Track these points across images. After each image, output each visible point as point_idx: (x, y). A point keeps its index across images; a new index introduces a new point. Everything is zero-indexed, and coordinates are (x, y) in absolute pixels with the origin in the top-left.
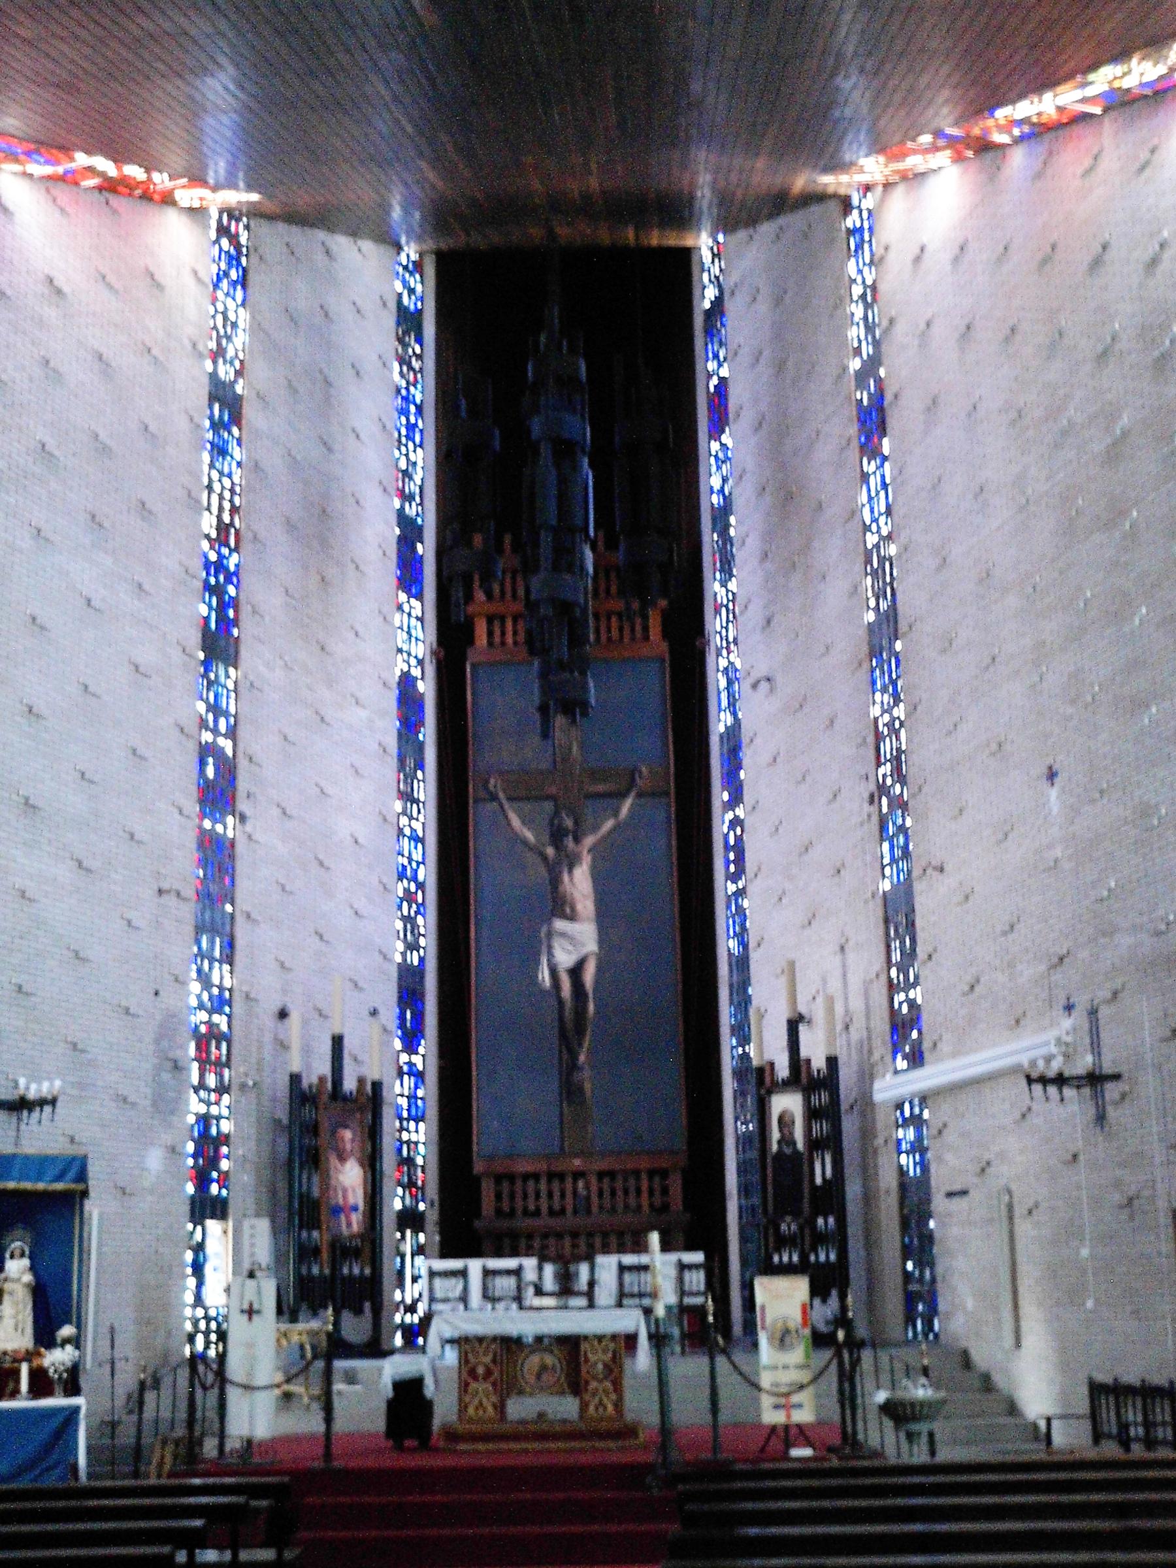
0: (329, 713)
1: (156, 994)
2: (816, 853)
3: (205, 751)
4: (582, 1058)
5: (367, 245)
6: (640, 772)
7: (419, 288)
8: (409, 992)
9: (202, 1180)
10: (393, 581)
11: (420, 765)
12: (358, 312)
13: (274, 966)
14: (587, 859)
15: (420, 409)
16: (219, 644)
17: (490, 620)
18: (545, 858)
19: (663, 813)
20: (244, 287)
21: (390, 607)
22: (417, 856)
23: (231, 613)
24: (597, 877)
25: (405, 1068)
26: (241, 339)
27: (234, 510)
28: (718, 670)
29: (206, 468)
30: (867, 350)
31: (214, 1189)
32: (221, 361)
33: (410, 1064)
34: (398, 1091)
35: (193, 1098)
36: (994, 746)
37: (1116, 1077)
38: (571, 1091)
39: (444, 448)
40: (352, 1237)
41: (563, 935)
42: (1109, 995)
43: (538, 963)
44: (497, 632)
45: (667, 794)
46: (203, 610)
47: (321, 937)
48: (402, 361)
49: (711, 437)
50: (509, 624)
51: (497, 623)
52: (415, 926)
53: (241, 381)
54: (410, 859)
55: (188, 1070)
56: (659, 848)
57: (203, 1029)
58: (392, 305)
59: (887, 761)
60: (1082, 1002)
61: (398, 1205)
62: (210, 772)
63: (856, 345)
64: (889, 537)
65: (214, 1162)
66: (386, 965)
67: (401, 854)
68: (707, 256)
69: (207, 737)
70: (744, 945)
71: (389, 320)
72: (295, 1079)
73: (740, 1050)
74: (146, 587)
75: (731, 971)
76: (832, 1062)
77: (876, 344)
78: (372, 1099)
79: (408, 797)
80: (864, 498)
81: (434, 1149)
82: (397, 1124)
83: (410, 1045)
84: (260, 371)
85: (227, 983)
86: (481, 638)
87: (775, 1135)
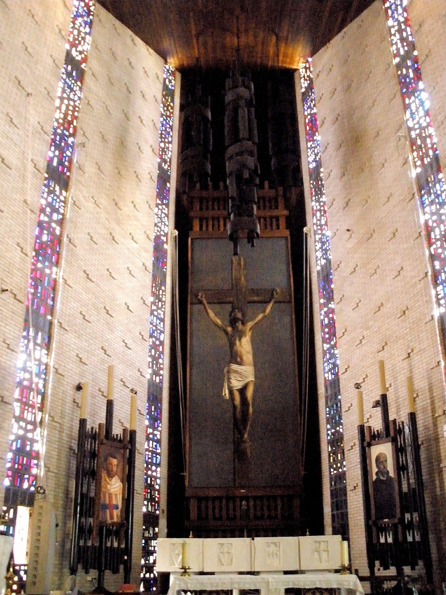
4: (246, 436)
5: (151, 51)
6: (276, 290)
7: (173, 81)
8: (154, 398)
10: (155, 194)
14: (249, 334)
17: (201, 220)
20: (90, 27)
21: (153, 205)
29: (60, 90)
35: (16, 426)
38: (239, 454)
39: (180, 161)
40: (113, 524)
41: (236, 372)
43: (222, 386)
45: (290, 302)
46: (51, 154)
49: (307, 141)
50: (211, 223)
51: (204, 221)
61: (144, 509)
65: (27, 468)
68: (302, 71)
69: (43, 218)
70: (336, 375)
72: (83, 422)
74: (14, 121)
76: (413, 416)
78: (128, 442)
87: (375, 469)
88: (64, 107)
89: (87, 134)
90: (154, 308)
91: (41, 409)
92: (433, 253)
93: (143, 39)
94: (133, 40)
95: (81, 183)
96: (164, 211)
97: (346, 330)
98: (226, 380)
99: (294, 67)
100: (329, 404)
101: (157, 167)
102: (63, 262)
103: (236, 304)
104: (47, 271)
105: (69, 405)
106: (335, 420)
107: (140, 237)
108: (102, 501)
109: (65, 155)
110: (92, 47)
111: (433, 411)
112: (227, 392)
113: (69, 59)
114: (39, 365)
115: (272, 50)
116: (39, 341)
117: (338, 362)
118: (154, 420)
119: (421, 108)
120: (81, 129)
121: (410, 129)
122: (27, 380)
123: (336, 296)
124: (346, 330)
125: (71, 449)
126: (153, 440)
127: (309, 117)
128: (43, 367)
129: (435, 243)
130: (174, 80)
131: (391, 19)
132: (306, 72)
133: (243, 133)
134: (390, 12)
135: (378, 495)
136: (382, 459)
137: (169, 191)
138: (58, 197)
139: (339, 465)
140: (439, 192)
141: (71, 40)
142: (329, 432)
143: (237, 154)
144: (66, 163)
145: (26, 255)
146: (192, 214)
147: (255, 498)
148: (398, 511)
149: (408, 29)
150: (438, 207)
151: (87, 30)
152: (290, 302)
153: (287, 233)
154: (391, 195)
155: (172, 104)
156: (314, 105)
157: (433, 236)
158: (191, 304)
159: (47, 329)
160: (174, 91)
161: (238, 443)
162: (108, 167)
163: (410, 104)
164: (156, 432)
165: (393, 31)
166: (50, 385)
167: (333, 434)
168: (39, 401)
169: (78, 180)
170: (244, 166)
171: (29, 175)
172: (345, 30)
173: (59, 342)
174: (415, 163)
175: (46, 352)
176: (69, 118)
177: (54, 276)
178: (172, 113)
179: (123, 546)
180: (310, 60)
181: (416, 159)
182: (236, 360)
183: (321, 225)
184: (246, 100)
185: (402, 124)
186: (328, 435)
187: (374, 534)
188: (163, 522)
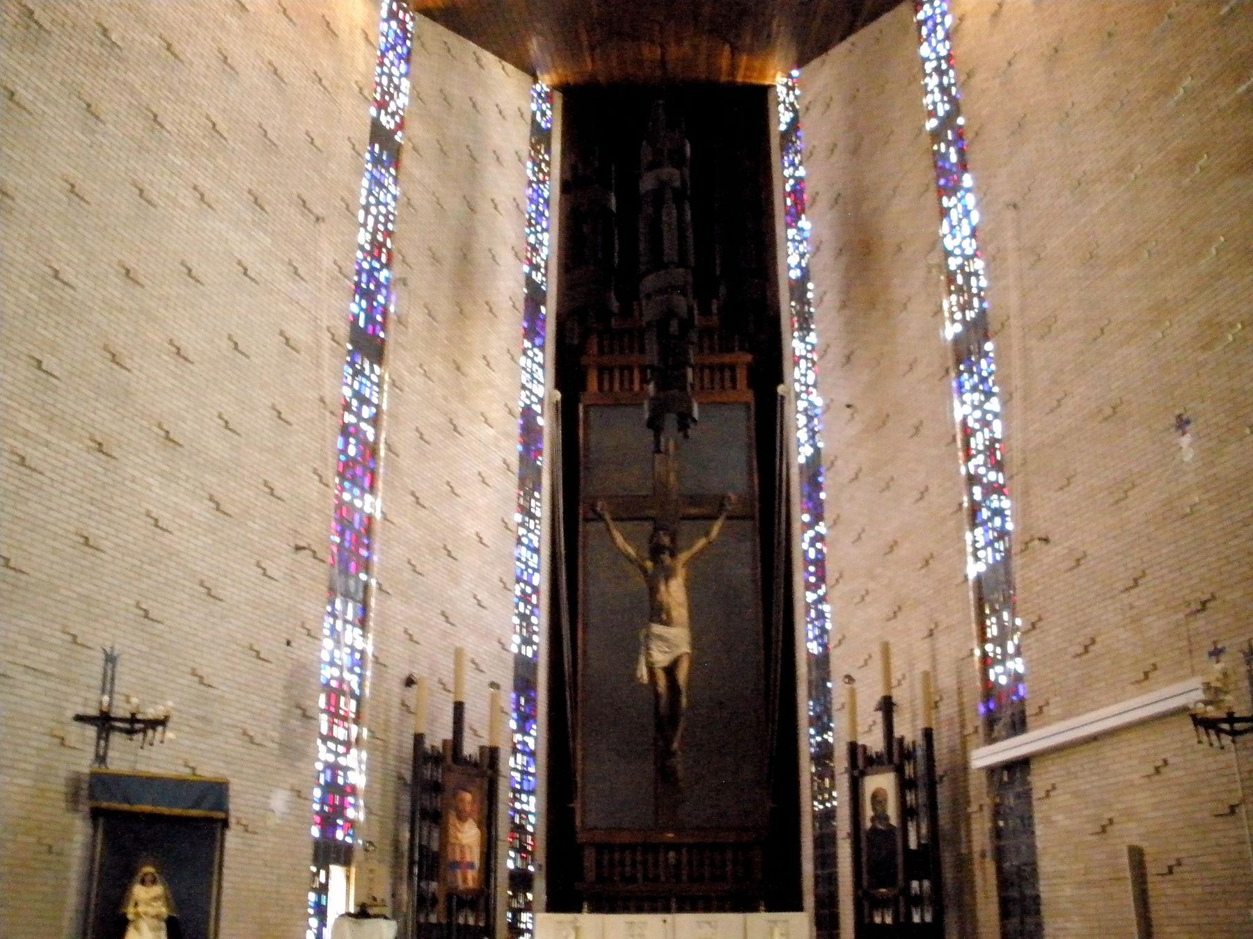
0: (461, 424)
1: (288, 643)
2: (903, 551)
4: (675, 745)
7: (549, 113)
8: (524, 684)
9: (327, 823)
11: (537, 486)
12: (500, 112)
15: (547, 202)
16: (368, 344)
18: (645, 571)
20: (408, 61)
21: (516, 351)
24: (690, 587)
26: (402, 101)
29: (364, 192)
30: (942, 109)
31: (339, 835)
32: (383, 112)
33: (525, 744)
34: (512, 764)
36: (1108, 411)
38: (665, 774)
40: (468, 891)
41: (660, 637)
43: (636, 661)
46: (354, 308)
48: (536, 163)
49: (788, 226)
50: (617, 375)
52: (530, 624)
53: (400, 133)
56: (742, 569)
58: (529, 121)
61: (510, 865)
65: (339, 811)
66: (504, 654)
68: (781, 91)
69: (349, 418)
70: (825, 646)
71: (526, 130)
72: (419, 739)
73: (819, 739)
74: (301, 271)
75: (810, 671)
76: (928, 734)
77: (953, 101)
79: (527, 512)
81: (543, 821)
82: (511, 795)
86: (593, 385)
88: (371, 220)
89: (410, 259)
90: (522, 531)
91: (357, 721)
92: (972, 472)
93: (495, 53)
94: (478, 60)
95: (403, 347)
96: (536, 359)
97: (841, 576)
99: (767, 82)
100: (814, 693)
101: (523, 282)
102: (380, 484)
104: (358, 503)
105: (395, 712)
106: (822, 722)
107: (497, 413)
108: (450, 857)
109: (375, 304)
110: (411, 98)
111: (963, 726)
113: (378, 134)
114: (352, 654)
115: (724, 63)
116: (350, 616)
117: (828, 626)
118: (525, 720)
119: (965, 221)
120: (400, 252)
121: (948, 254)
123: (827, 514)
124: (841, 576)
125: (400, 777)
126: (523, 753)
127: (791, 182)
128: (357, 656)
129: (975, 456)
130: (551, 109)
131: (925, 44)
132: (788, 95)
134: (924, 31)
135: (876, 849)
136: (880, 798)
137: (544, 321)
139: (827, 796)
140: (985, 374)
141: (378, 97)
142: (812, 741)
144: (379, 318)
145: (327, 485)
146: (584, 360)
147: (690, 847)
148: (900, 876)
149: (951, 73)
150: (983, 398)
151: (403, 68)
152: (753, 518)
153: (749, 396)
155: (547, 157)
156: (801, 163)
157: (973, 445)
159: (361, 595)
160: (549, 131)
161: (663, 755)
162: (444, 308)
163: (949, 209)
165: (929, 67)
166: (368, 683)
167: (819, 744)
168: (354, 709)
169: (397, 342)
171: (326, 354)
172: (852, 38)
173: (380, 614)
174: (952, 313)
175: (360, 632)
178: (549, 174)
179: (482, 924)
180: (795, 73)
181: (955, 309)
182: (659, 615)
183: (808, 386)
185: (938, 240)
186: (811, 745)
187: (866, 911)
188: (540, 884)
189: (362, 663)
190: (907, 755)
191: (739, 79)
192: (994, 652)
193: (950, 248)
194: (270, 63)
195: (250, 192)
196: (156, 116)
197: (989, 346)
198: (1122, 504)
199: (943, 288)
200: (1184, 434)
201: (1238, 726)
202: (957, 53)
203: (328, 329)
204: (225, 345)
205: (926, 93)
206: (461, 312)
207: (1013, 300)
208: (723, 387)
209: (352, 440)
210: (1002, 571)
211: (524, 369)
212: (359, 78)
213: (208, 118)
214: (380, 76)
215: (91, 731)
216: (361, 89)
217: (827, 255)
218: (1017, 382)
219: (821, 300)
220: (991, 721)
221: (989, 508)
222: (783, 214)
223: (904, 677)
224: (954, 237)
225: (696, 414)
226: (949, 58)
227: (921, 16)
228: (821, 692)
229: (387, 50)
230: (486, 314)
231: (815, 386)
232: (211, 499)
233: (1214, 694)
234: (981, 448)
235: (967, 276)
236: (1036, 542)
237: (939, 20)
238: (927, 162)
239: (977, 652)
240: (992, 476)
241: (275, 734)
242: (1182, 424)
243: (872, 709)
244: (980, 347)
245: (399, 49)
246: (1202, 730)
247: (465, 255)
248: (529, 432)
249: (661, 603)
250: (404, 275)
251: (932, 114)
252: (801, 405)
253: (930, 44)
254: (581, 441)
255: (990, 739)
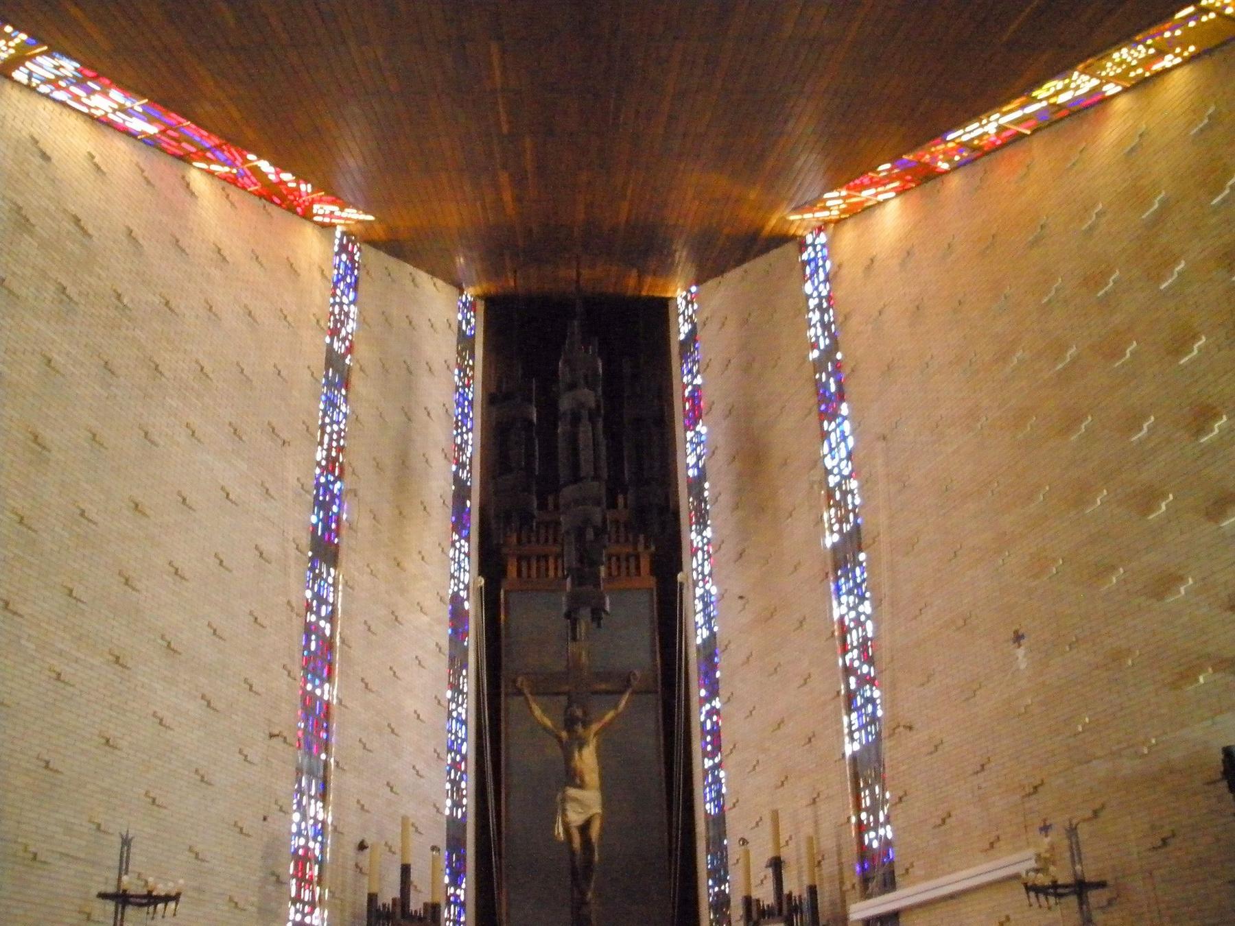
0: (401, 614)
1: (265, 819)
3: (309, 629)
4: (590, 895)
5: (440, 283)
7: (473, 320)
8: (455, 842)
11: (465, 666)
13: (355, 806)
15: (471, 403)
16: (325, 550)
17: (519, 559)
18: (560, 739)
19: (653, 703)
20: (355, 290)
21: (447, 544)
22: (462, 734)
23: (333, 526)
24: (601, 755)
25: (452, 899)
26: (351, 326)
27: (340, 449)
28: (695, 598)
30: (823, 343)
33: (457, 897)
36: (961, 623)
37: (1102, 885)
41: (575, 800)
42: (1089, 814)
44: (524, 569)
46: (314, 519)
47: (392, 789)
48: (462, 369)
49: (687, 429)
52: (459, 790)
54: (457, 737)
55: (288, 884)
56: (648, 742)
57: (301, 852)
58: (456, 330)
59: (853, 648)
60: (1059, 821)
62: (313, 646)
63: (813, 340)
64: (850, 476)
67: (450, 731)
68: (681, 303)
70: (721, 808)
71: (453, 339)
72: (372, 898)
74: (272, 492)
75: (708, 829)
76: (813, 890)
77: (833, 337)
79: (456, 688)
80: (826, 449)
83: (455, 882)
84: (362, 350)
85: (320, 817)
88: (326, 438)
98: (560, 811)
99: (669, 295)
103: (576, 695)
104: (318, 692)
106: (719, 874)
107: (430, 602)
111: (842, 883)
112: (561, 829)
119: (842, 445)
121: (828, 472)
122: (303, 847)
126: (455, 903)
127: (690, 388)
128: (320, 826)
133: (586, 468)
138: (326, 581)
143: (577, 502)
149: (831, 312)
153: (652, 582)
154: (799, 563)
156: (698, 372)
158: (507, 695)
161: (579, 904)
163: (829, 433)
164: (458, 892)
165: (813, 303)
167: (716, 894)
170: (587, 521)
171: (292, 562)
172: (746, 266)
174: (831, 525)
176: (334, 454)
177: (326, 697)
178: (473, 377)
180: (694, 289)
181: (833, 521)
184: (590, 409)
189: (322, 832)
190: (795, 909)
191: (644, 293)
192: (868, 819)
193: (829, 468)
194: (246, 306)
195: (230, 424)
196: (157, 366)
197: (862, 557)
198: (972, 701)
199: (823, 501)
200: (1019, 646)
201: (1060, 891)
202: (839, 294)
203: (294, 540)
204: (212, 562)
205: (810, 327)
206: (401, 513)
207: (883, 519)
208: (628, 574)
209: (313, 637)
210: (873, 752)
211: (454, 559)
212: (315, 310)
213: (197, 362)
214: (333, 305)
215: (110, 906)
216: (318, 321)
217: (721, 456)
218: (885, 590)
219: (716, 501)
220: (865, 881)
221: (862, 696)
222: (682, 417)
223: (791, 838)
224: (833, 458)
225: (608, 608)
226: (829, 298)
227: (805, 257)
228: (717, 848)
229: (339, 281)
230: (422, 513)
231: (710, 574)
232: (203, 697)
233: (1043, 864)
234: (855, 644)
235: (845, 494)
236: (901, 729)
237: (821, 263)
238: (811, 389)
239: (853, 820)
240: (865, 669)
241: (254, 899)
242: (1018, 638)
243: (764, 865)
244: (855, 556)
245: (348, 280)
246: (1032, 894)
247: (403, 462)
248: (457, 616)
249: (574, 770)
250: (353, 487)
251: (815, 346)
252: (699, 592)
253: (813, 283)
254: (502, 622)
255: (866, 895)
